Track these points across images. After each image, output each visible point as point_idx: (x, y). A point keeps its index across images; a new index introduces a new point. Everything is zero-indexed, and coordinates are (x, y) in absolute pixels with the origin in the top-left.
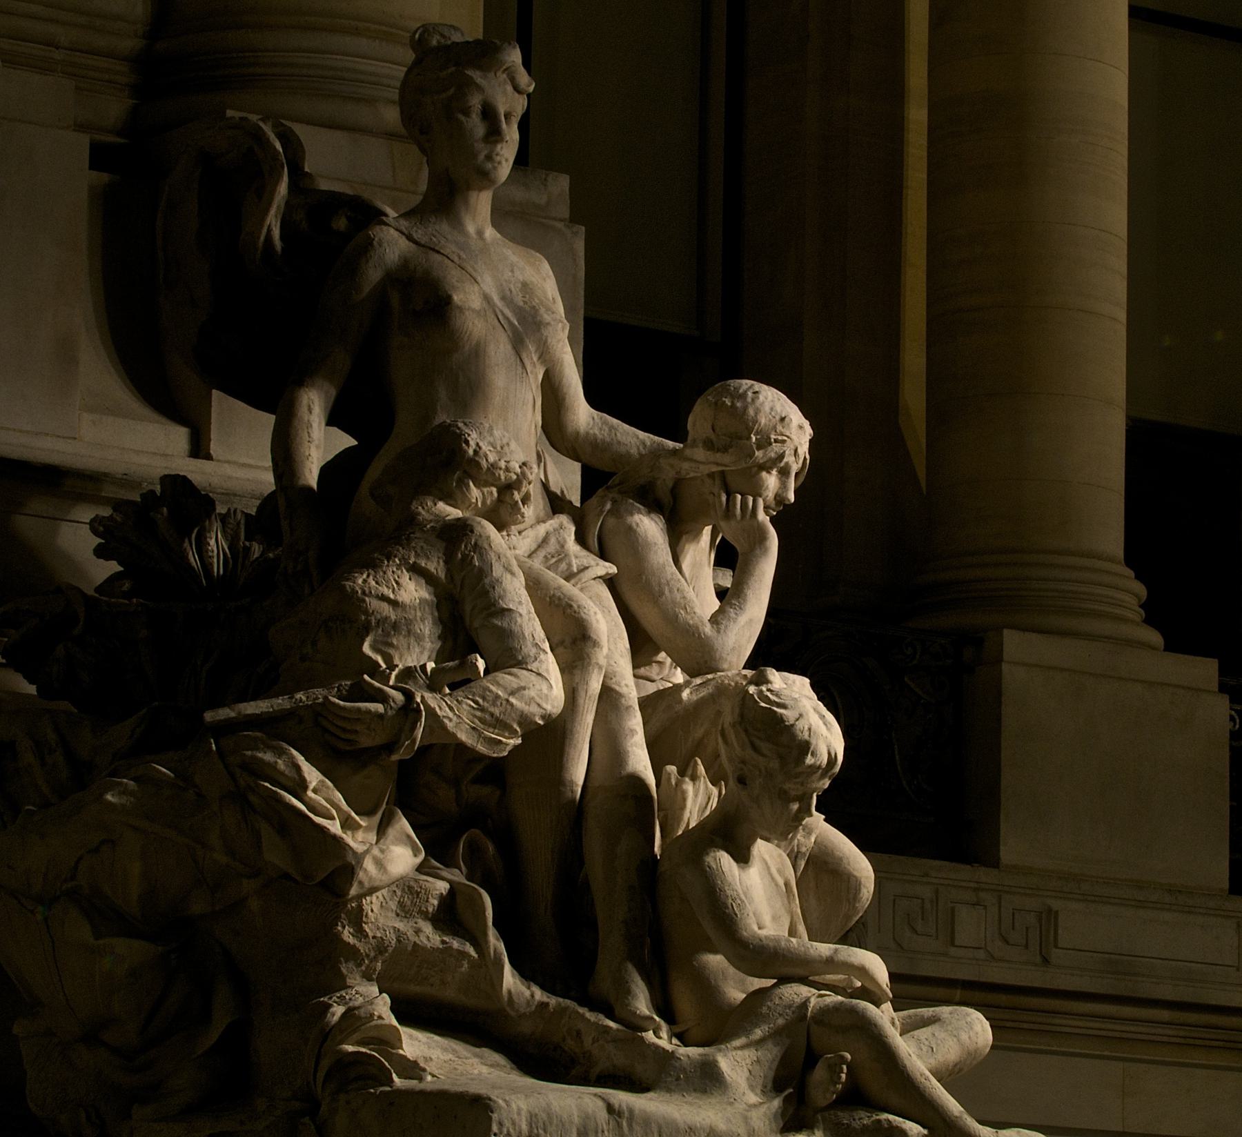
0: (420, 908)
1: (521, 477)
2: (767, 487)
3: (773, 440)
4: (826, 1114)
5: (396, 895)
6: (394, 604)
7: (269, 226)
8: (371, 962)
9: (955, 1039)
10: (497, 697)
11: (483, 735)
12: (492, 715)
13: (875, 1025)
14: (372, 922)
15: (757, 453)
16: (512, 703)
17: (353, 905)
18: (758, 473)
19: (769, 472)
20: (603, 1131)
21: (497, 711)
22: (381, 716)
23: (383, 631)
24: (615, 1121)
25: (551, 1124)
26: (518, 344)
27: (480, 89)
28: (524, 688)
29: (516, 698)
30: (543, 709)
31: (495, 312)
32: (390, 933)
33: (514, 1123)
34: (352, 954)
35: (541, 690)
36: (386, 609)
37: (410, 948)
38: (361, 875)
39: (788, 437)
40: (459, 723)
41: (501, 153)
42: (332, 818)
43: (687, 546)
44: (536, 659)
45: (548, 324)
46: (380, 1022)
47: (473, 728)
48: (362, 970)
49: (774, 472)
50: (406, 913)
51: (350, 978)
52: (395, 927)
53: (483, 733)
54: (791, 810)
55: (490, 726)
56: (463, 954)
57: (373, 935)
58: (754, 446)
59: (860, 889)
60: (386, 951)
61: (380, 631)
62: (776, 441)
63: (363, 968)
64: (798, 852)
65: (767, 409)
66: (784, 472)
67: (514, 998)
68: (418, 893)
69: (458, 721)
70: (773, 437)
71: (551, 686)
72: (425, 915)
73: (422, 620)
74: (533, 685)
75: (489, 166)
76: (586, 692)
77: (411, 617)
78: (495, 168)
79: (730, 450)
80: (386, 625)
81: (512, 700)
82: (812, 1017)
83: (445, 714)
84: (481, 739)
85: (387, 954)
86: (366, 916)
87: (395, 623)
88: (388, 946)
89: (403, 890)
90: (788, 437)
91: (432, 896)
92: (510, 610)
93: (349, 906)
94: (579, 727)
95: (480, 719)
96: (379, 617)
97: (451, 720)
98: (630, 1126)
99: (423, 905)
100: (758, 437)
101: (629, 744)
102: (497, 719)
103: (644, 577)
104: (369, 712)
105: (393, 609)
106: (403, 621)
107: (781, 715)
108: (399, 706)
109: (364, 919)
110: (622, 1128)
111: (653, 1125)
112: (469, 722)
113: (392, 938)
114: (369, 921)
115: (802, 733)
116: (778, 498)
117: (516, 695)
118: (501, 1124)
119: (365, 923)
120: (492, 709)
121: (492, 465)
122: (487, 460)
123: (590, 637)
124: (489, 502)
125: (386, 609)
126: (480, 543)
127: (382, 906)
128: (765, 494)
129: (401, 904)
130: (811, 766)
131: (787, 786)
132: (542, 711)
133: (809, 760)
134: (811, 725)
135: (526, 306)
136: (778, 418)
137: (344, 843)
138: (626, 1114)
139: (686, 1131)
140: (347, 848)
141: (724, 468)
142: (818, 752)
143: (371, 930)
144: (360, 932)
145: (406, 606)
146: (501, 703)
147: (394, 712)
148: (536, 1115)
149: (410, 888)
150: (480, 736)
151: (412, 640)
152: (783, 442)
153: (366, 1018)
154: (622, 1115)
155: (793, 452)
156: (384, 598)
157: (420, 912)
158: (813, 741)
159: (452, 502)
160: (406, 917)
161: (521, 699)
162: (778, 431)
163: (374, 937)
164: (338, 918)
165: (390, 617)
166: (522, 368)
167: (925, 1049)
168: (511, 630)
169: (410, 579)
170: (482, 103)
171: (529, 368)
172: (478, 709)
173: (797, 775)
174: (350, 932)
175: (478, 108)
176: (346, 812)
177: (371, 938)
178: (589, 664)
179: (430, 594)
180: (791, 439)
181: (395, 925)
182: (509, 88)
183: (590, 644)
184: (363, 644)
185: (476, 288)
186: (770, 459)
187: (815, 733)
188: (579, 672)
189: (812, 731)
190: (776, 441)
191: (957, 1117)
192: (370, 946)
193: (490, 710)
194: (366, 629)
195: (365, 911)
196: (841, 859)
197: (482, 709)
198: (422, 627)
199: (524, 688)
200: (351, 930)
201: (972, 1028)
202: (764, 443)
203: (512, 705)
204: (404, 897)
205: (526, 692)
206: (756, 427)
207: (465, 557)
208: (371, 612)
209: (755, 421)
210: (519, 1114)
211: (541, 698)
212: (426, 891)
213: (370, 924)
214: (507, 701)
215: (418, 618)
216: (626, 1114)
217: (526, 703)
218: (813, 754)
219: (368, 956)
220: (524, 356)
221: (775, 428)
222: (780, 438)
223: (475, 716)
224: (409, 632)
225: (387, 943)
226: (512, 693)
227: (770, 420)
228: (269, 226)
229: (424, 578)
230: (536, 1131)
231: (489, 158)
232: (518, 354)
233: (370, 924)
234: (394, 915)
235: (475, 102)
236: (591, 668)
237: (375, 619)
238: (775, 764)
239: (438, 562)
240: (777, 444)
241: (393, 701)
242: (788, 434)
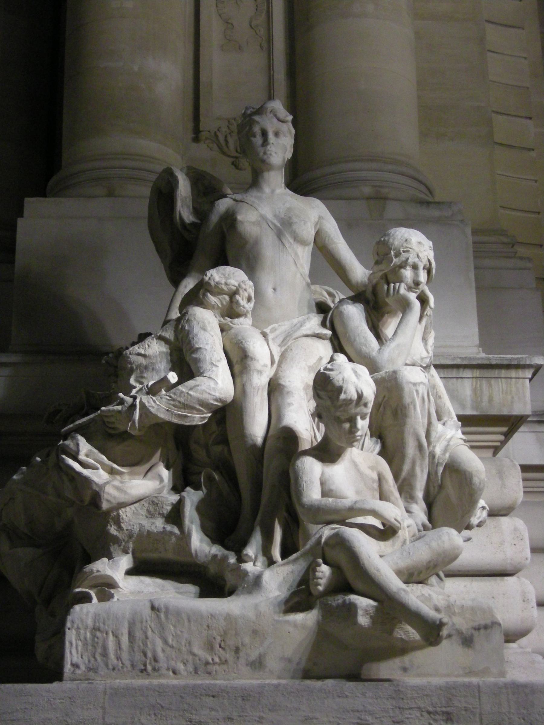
0: (159, 511)
1: (238, 288)
2: (406, 277)
3: (402, 251)
4: (322, 599)
5: (144, 506)
6: (144, 356)
7: (179, 211)
8: (126, 543)
9: (427, 546)
10: (182, 392)
11: (174, 413)
12: (180, 402)
13: (348, 541)
14: (126, 522)
15: (394, 260)
16: (191, 394)
17: (114, 514)
18: (399, 270)
19: (405, 269)
20: (147, 621)
21: (182, 400)
22: (119, 412)
23: (140, 371)
24: (155, 614)
25: (108, 619)
26: (279, 235)
27: (258, 123)
28: (198, 386)
29: (193, 391)
30: (214, 395)
31: (267, 222)
32: (136, 527)
33: (82, 621)
34: (116, 540)
35: (209, 385)
36: (141, 360)
37: (145, 533)
38: (105, 496)
39: (411, 248)
40: (159, 408)
41: (270, 149)
42: (97, 469)
43: (389, 320)
44: (210, 370)
45: (296, 222)
46: (98, 574)
47: (167, 410)
48: (121, 548)
49: (408, 268)
50: (152, 515)
51: (114, 554)
52: (140, 523)
53: (173, 412)
54: (344, 428)
55: (181, 408)
56: (171, 533)
57: (126, 529)
58: (393, 257)
59: (472, 478)
60: (133, 537)
61: (139, 371)
62: (404, 252)
63: (122, 547)
64: (438, 463)
65: (399, 237)
66: (415, 267)
67: (198, 553)
68: (157, 504)
69: (158, 407)
70: (402, 250)
71: (217, 383)
72: (162, 515)
73: (161, 362)
74: (204, 383)
75: (265, 157)
76: (251, 386)
77: (154, 362)
78: (268, 157)
79: (384, 262)
80: (141, 368)
81: (191, 393)
82: (326, 543)
83: (150, 405)
84: (173, 416)
85: (134, 538)
86: (122, 519)
87: (146, 366)
88: (134, 534)
89: (149, 503)
90: (411, 248)
91: (166, 505)
92: (200, 348)
93: (112, 514)
94: (249, 405)
95: (174, 406)
96: (137, 364)
97: (153, 407)
98: (167, 617)
99: (160, 510)
100: (395, 251)
101: (286, 411)
102: (184, 404)
103: (347, 334)
104: (114, 411)
105: (144, 359)
106: (150, 364)
107: (329, 374)
108: (129, 405)
109: (121, 521)
110: (161, 618)
111: (183, 615)
112: (164, 407)
113: (136, 529)
114: (124, 521)
115: (338, 382)
116: (415, 282)
117: (193, 390)
118: (73, 622)
119: (122, 523)
120: (179, 399)
121: (217, 283)
122: (214, 281)
123: (248, 356)
124: (224, 303)
125: (141, 360)
126: (190, 318)
127: (134, 513)
128: (406, 280)
129: (148, 511)
130: (344, 400)
131: (338, 414)
132: (212, 396)
133: (343, 396)
134: (344, 377)
135: (286, 217)
136: (404, 240)
137: (91, 480)
138: (163, 610)
139: (208, 617)
140: (92, 482)
141: (384, 272)
142: (348, 391)
143: (126, 526)
144: (120, 528)
145: (151, 356)
146: (184, 395)
147: (127, 408)
148: (99, 615)
149: (153, 502)
150: (172, 414)
151: (154, 372)
152: (408, 251)
153: (89, 572)
154: (160, 610)
155: (417, 256)
156: (139, 354)
157: (159, 514)
158: (345, 386)
159: (203, 306)
160: (151, 518)
161: (196, 392)
162: (404, 246)
163: (127, 530)
164: (108, 522)
165: (142, 363)
166: (283, 246)
167: (405, 554)
168: (200, 358)
169: (157, 343)
170: (260, 129)
171: (287, 245)
172: (171, 400)
173: (340, 406)
174: (115, 529)
175: (259, 132)
176: (108, 465)
177: (125, 530)
178: (250, 370)
179: (167, 349)
180: (413, 249)
181: (140, 522)
182: (275, 121)
183: (249, 359)
184: (129, 379)
185: (256, 212)
186: (403, 262)
187: (346, 381)
188: (245, 375)
189: (345, 380)
190: (404, 252)
191: (395, 592)
192: (125, 535)
193: (178, 399)
194: (131, 371)
195: (121, 516)
196: (460, 463)
197: (174, 400)
198: (160, 366)
199: (198, 386)
200: (116, 528)
201: (440, 539)
202: (398, 255)
203: (191, 395)
204: (149, 507)
205: (199, 388)
206: (393, 247)
207: (182, 326)
208: (132, 362)
209: (392, 244)
210: (87, 615)
211: (210, 390)
212: (162, 502)
213: (125, 523)
214: (188, 393)
215: (158, 362)
216: (163, 610)
217: (200, 394)
218: (345, 393)
219: (124, 540)
220: (284, 240)
221: (402, 246)
222: (405, 249)
223: (170, 404)
224: (153, 369)
225: (133, 532)
226: (191, 389)
227: (400, 242)
228: (179, 211)
229: (164, 341)
230: (97, 624)
231: (265, 153)
232: (280, 239)
233: (125, 523)
234: (144, 517)
235: (257, 129)
236: (251, 372)
237: (135, 366)
238: (328, 403)
239: (171, 332)
240: (405, 253)
241: (127, 403)
242: (410, 247)
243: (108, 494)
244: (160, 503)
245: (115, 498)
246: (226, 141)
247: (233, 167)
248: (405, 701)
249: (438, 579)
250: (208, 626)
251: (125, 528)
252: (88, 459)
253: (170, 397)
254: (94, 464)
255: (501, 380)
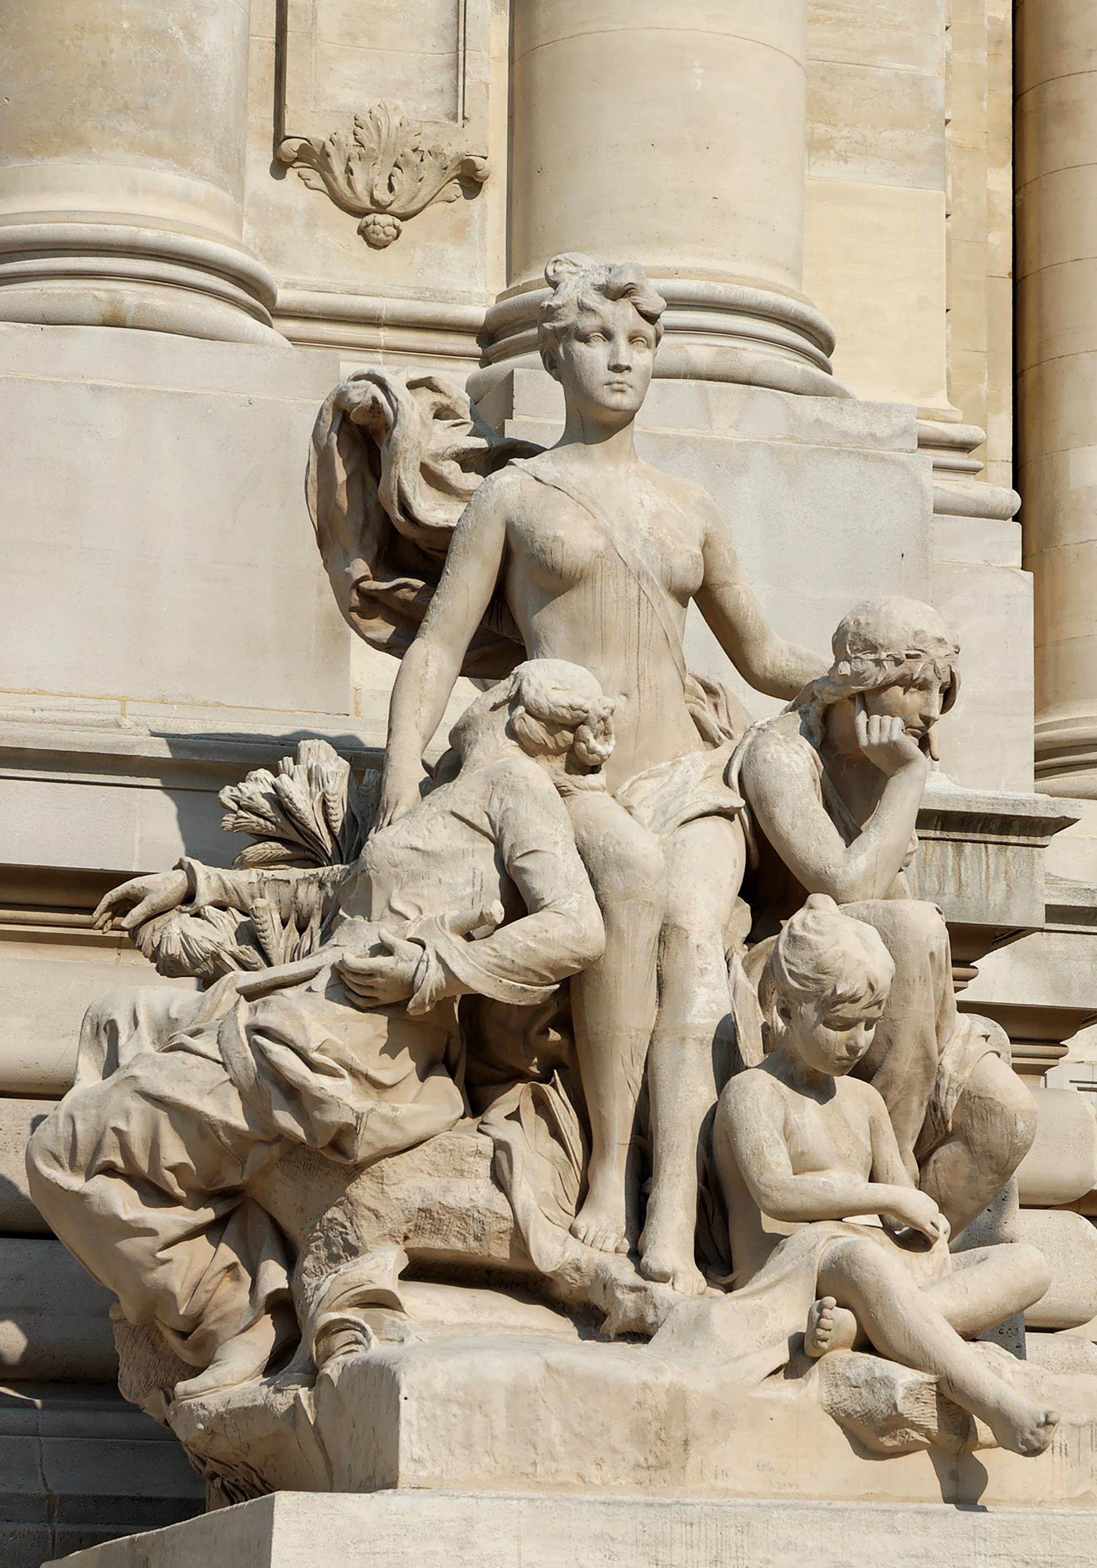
42: (342, 1076)
243: (374, 1131)
244: (457, 1149)
245: (381, 1138)
246: (349, 171)
247: (361, 238)
248: (988, 1543)
249: (274, 1216)
250: (639, 1403)
251: (392, 1196)
252: (323, 1057)
253: (494, 949)
254: (335, 1069)
255: (986, 848)
